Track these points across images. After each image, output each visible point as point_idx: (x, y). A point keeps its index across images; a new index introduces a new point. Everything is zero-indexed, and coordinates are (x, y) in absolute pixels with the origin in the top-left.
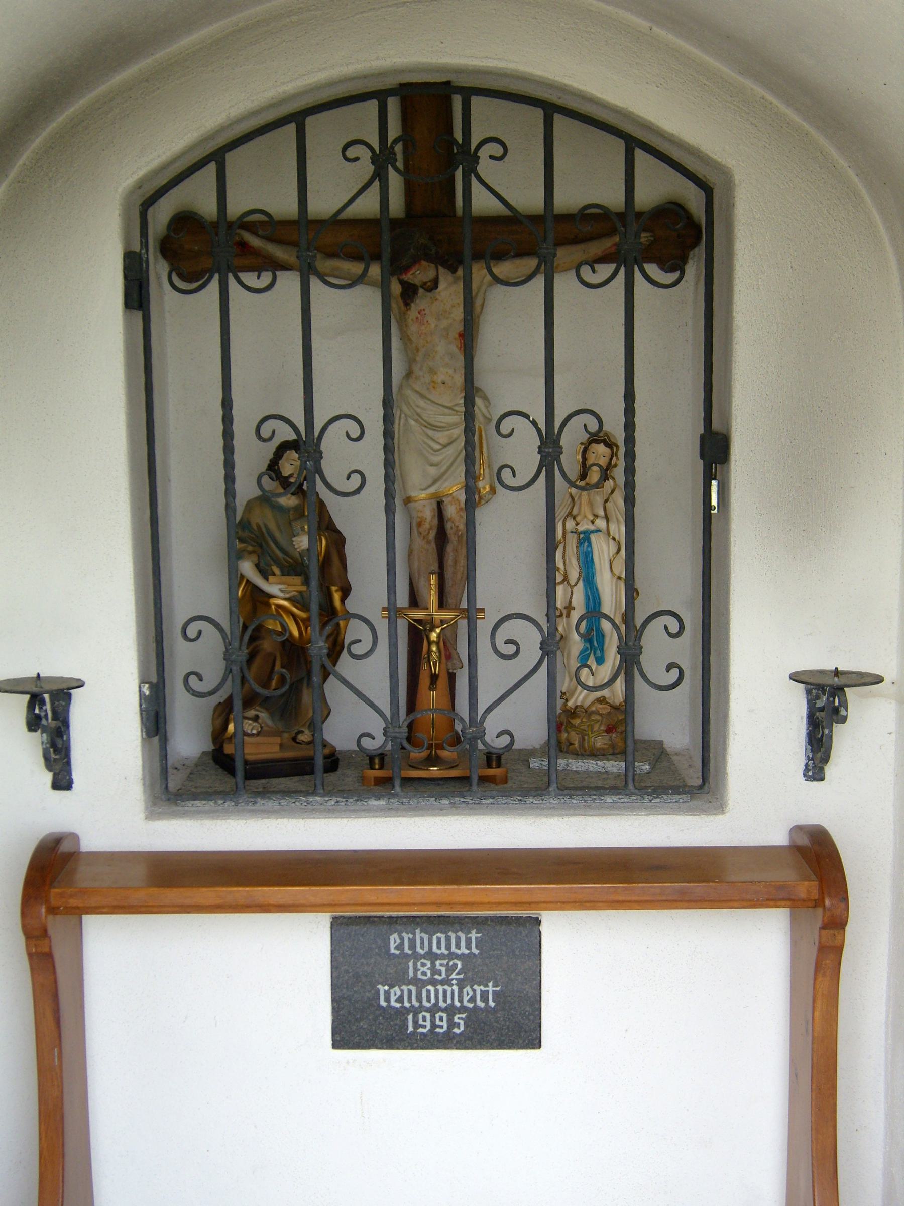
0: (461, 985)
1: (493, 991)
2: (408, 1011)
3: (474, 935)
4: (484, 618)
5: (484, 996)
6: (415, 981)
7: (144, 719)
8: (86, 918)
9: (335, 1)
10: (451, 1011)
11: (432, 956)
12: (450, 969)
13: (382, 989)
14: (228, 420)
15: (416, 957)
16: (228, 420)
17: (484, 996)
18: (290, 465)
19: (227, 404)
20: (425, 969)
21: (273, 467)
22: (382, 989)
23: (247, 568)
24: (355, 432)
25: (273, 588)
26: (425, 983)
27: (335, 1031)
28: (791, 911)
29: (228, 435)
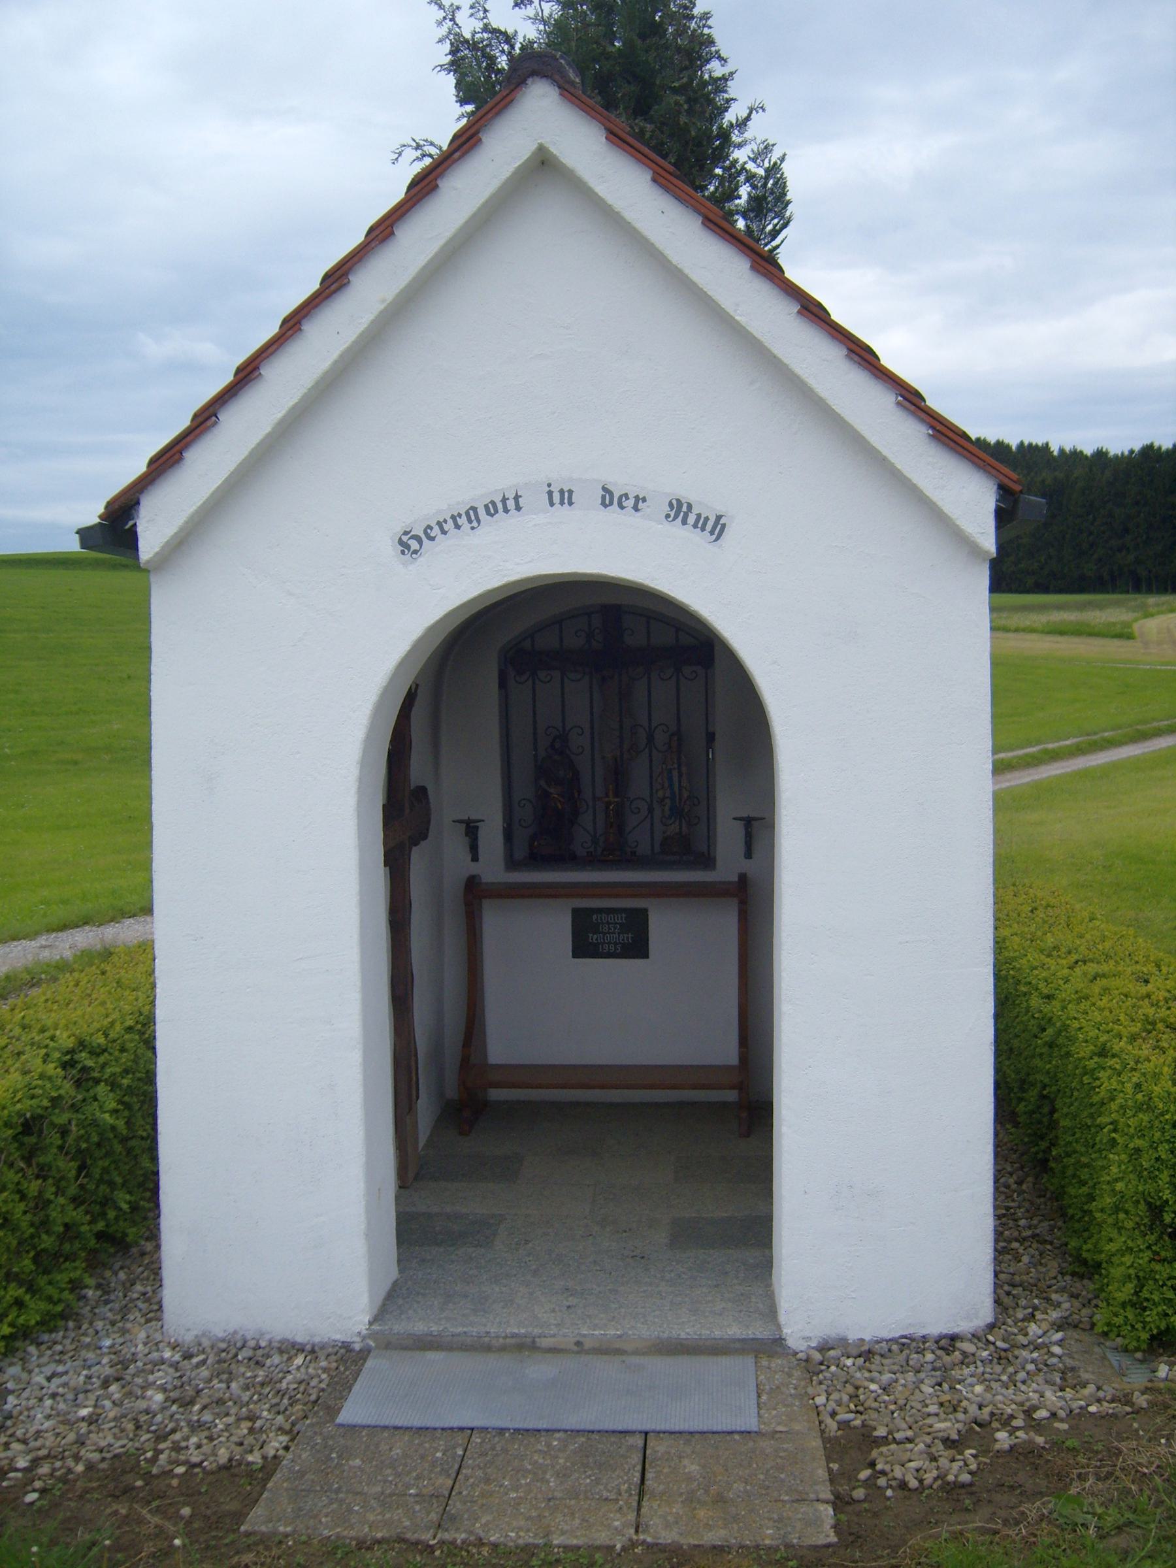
0: (619, 934)
1: (491, 99)
2: (598, 943)
3: (624, 915)
4: (552, 504)
5: (628, 938)
6: (602, 933)
7: (425, 1111)
8: (484, 901)
9: (668, 1567)
10: (616, 944)
11: (608, 923)
12: (615, 928)
13: (591, 935)
14: (535, 728)
15: (603, 923)
16: (535, 728)
17: (628, 938)
18: (557, 745)
19: (535, 722)
20: (606, 929)
21: (552, 746)
22: (591, 935)
23: (542, 783)
24: (580, 731)
25: (551, 790)
26: (605, 933)
27: (573, 951)
28: (730, 883)
29: (535, 734)
